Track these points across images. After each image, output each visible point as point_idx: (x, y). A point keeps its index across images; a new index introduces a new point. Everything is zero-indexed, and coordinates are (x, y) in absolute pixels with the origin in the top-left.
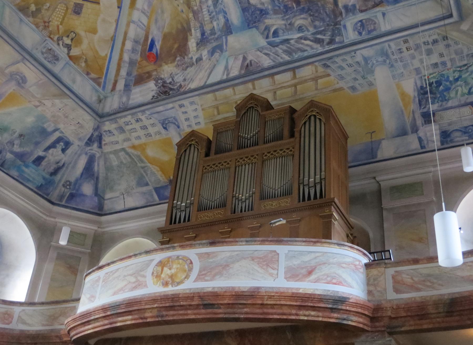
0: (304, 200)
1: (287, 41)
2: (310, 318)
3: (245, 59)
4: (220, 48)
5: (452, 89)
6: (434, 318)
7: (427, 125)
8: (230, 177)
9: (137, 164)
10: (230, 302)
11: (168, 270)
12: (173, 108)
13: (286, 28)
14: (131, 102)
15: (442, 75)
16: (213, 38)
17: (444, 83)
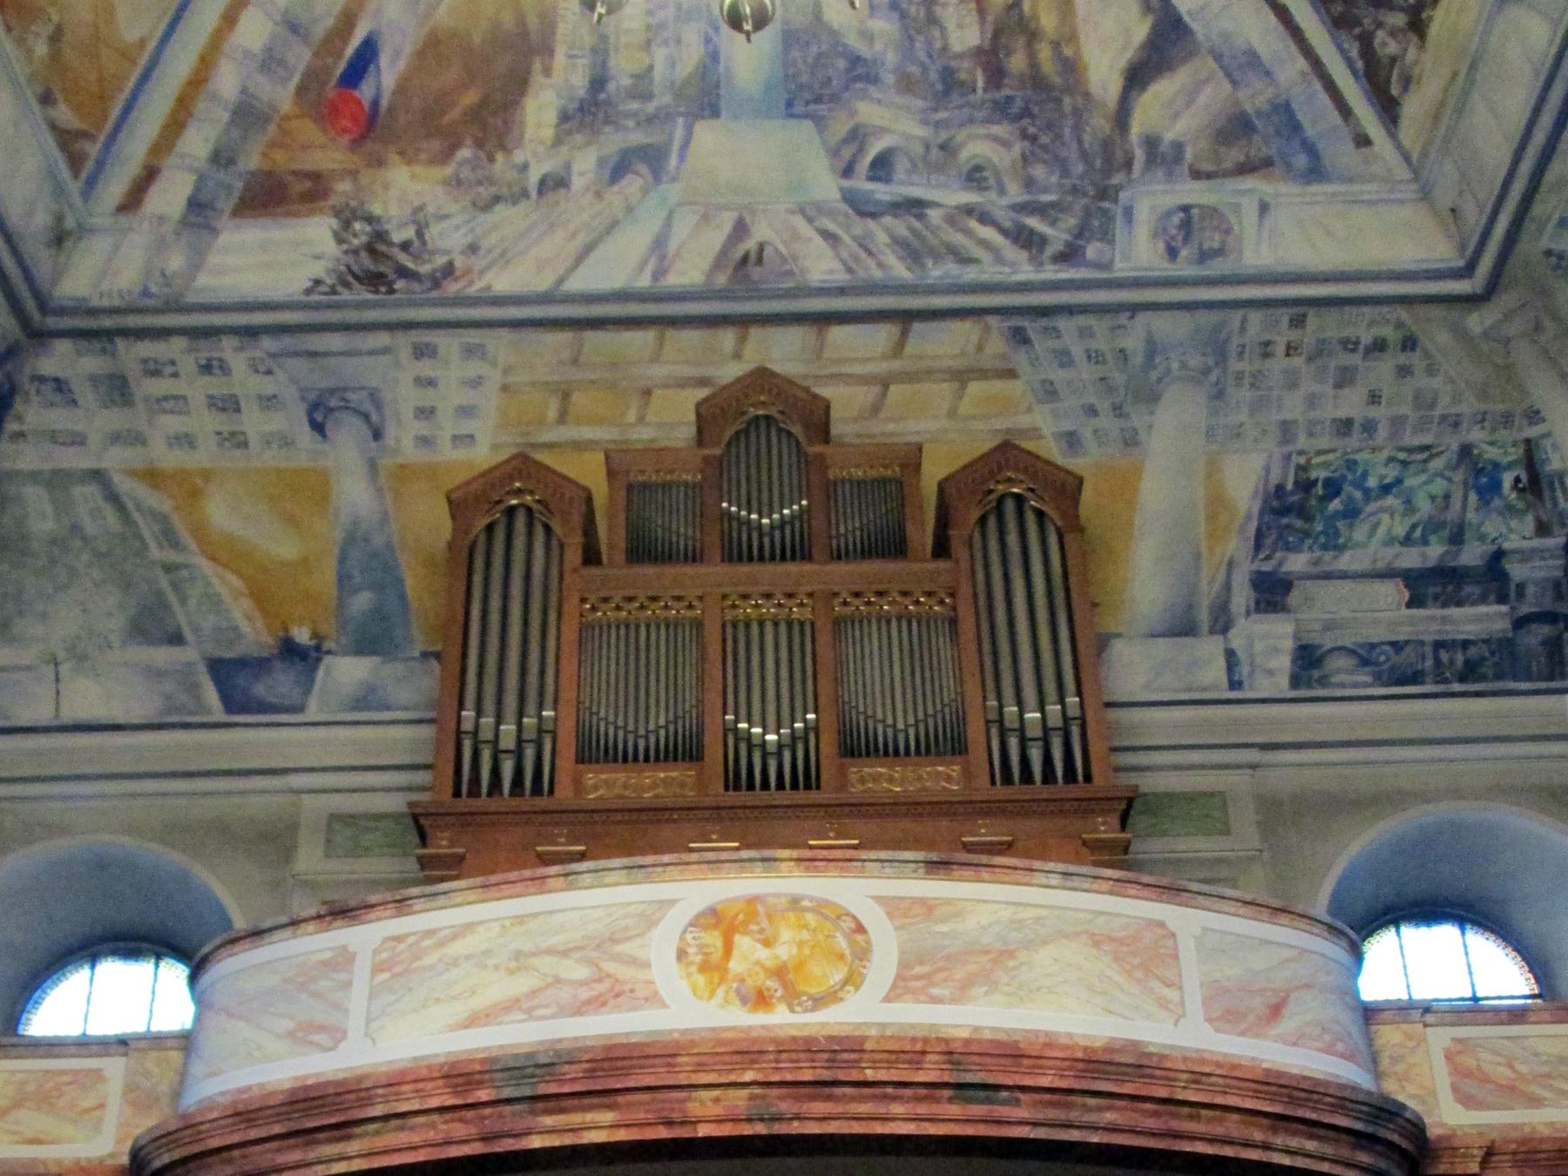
1: (915, 207)
2: (1300, 1163)
3: (741, 229)
4: (652, 159)
5: (1362, 516)
7: (1262, 616)
9: (145, 546)
11: (759, 946)
12: (385, 351)
13: (924, 158)
14: (203, 280)
15: (1351, 465)
16: (635, 115)
17: (1347, 488)
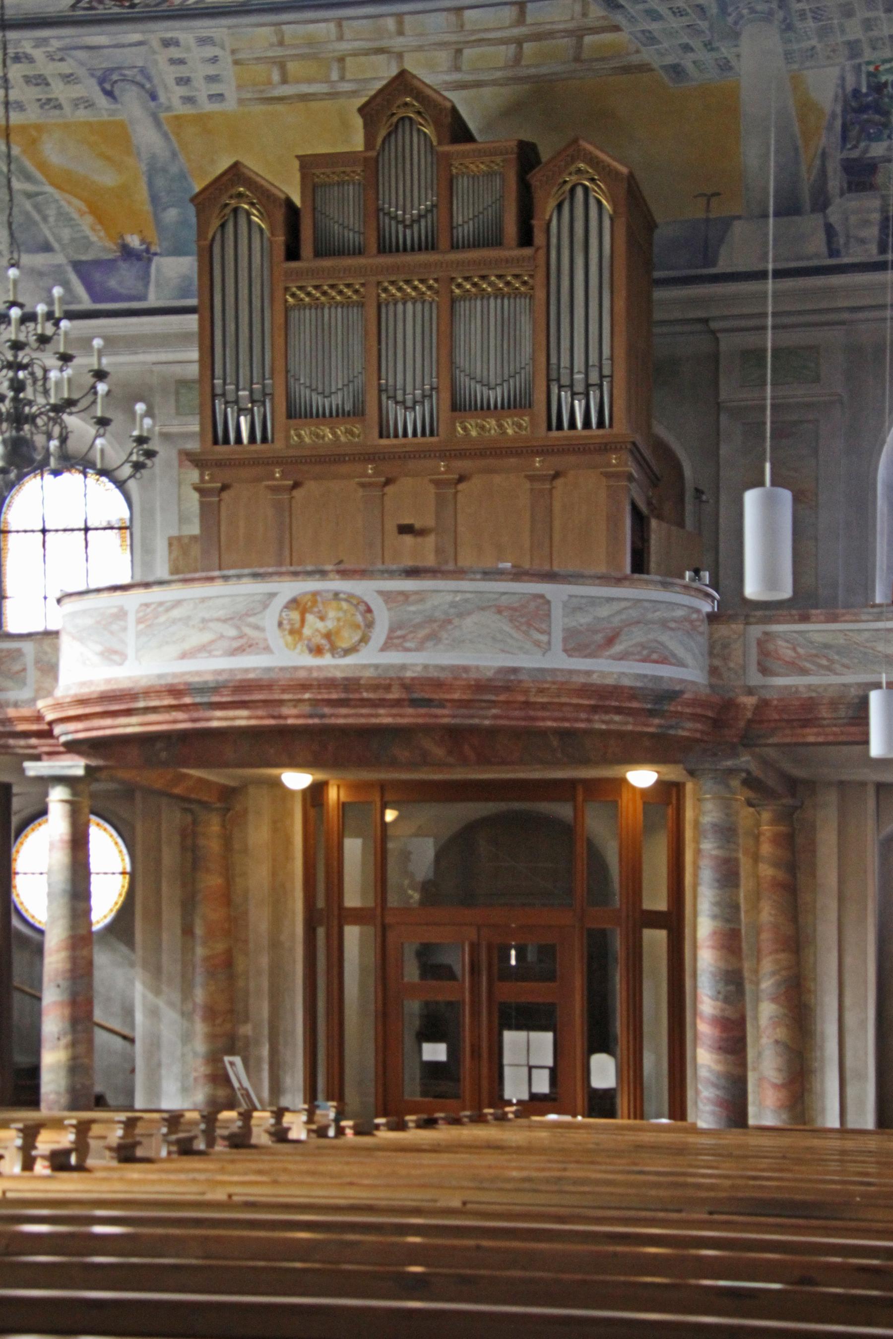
0: (560, 427)
6: (828, 726)
8: (366, 333)
10: (465, 697)
11: (318, 620)
